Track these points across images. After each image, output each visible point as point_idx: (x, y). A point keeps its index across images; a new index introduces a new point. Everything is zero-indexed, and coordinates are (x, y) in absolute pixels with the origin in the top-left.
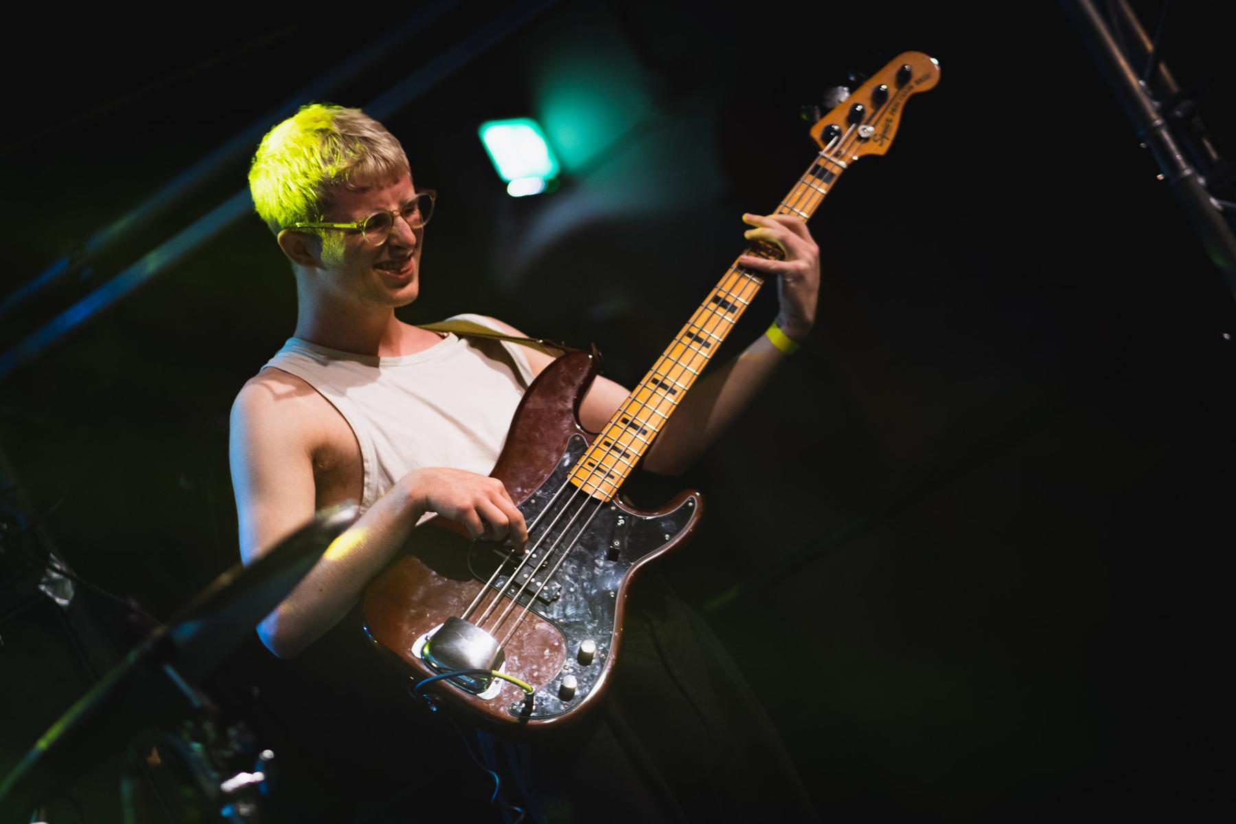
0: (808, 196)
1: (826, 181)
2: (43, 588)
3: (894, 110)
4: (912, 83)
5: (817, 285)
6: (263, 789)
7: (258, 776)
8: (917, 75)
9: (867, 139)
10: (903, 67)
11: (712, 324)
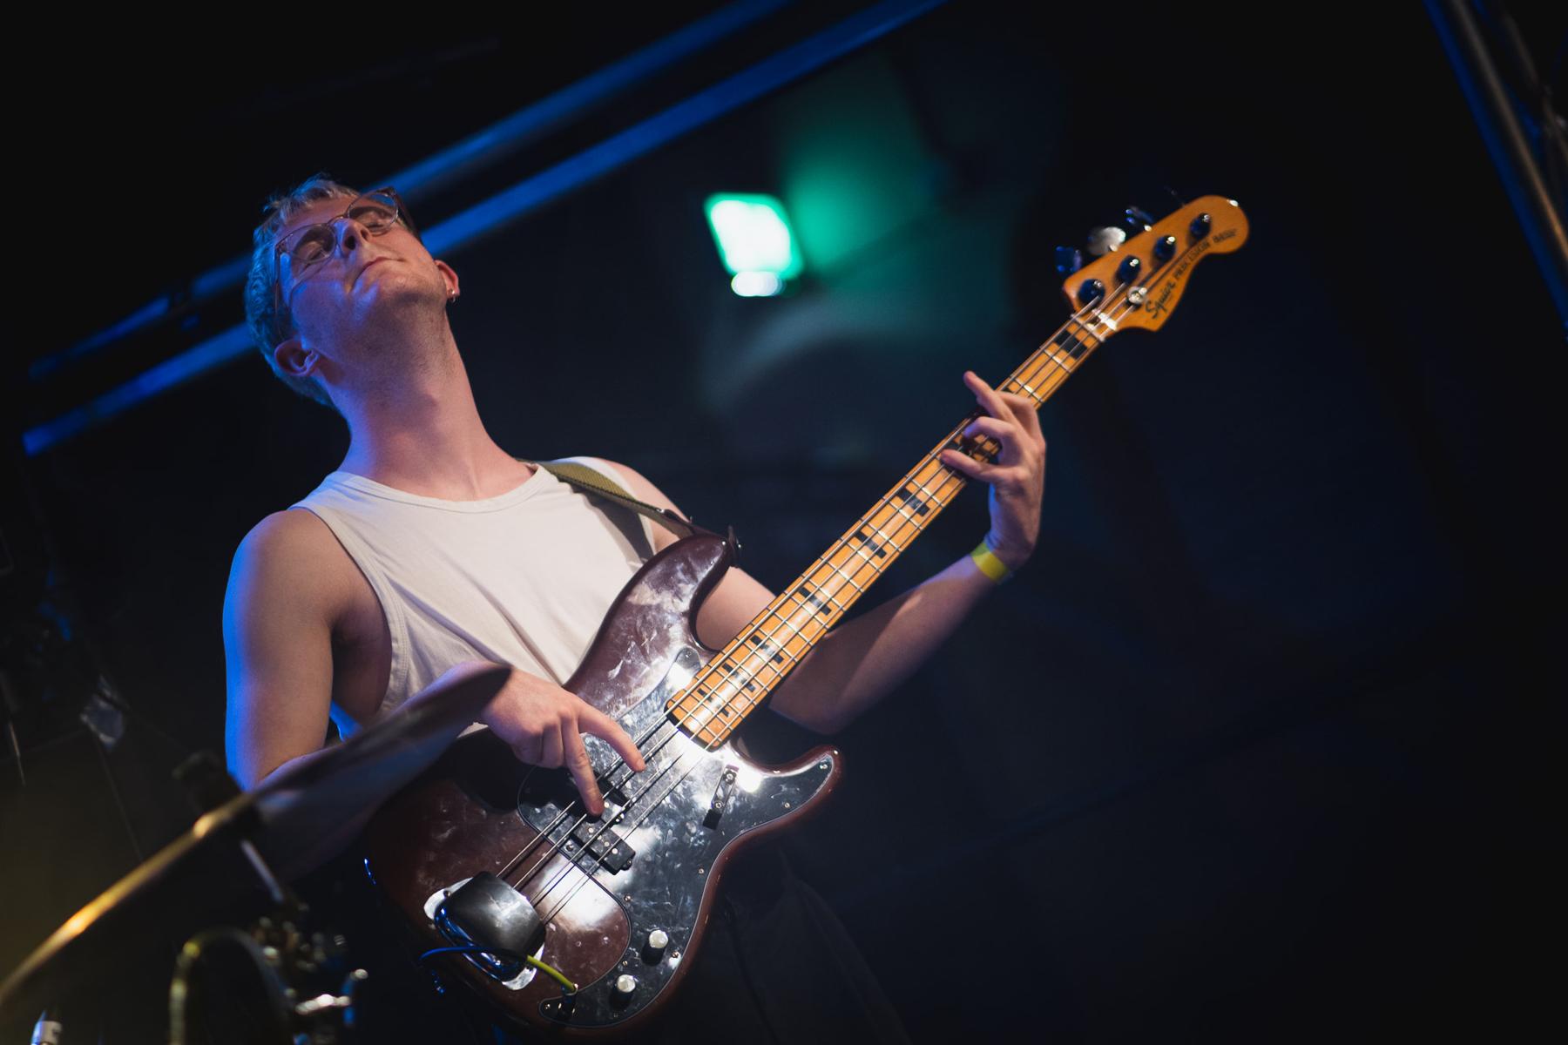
0: (1047, 370)
1: (1075, 355)
2: (85, 718)
3: (1180, 272)
4: (1210, 238)
5: (1040, 499)
6: (349, 1015)
7: (343, 1000)
8: (1217, 229)
9: (1137, 306)
10: (1202, 216)
11: (892, 525)
